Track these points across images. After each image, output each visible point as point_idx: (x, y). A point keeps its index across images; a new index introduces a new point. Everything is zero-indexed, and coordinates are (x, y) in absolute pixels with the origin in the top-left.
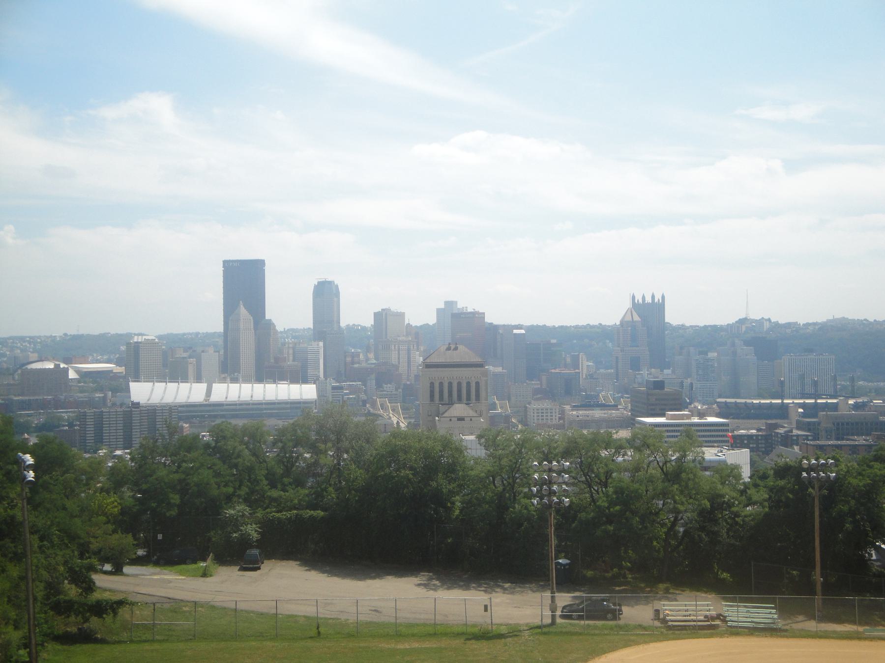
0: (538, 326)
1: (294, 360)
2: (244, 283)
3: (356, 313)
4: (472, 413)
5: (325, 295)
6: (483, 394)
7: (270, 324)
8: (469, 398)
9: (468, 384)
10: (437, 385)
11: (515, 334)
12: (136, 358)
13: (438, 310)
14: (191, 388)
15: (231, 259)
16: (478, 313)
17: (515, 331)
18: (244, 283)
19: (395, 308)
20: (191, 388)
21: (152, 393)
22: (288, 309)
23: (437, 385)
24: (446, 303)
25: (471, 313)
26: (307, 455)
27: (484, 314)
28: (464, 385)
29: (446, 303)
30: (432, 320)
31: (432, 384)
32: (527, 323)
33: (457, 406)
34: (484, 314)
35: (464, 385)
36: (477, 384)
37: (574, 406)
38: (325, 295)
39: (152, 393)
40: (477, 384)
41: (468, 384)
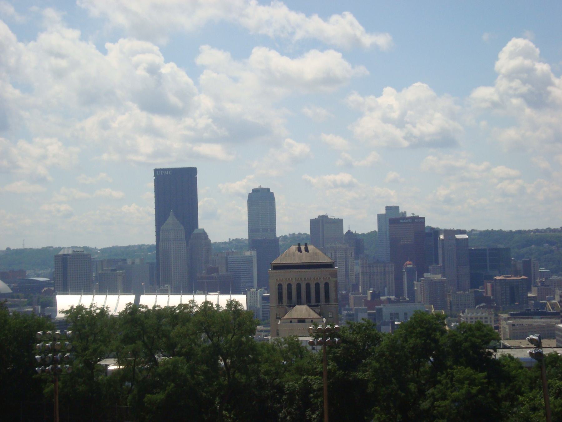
0: (493, 231)
1: (227, 271)
2: (176, 191)
3: (292, 221)
4: (314, 315)
5: (261, 202)
6: (332, 295)
7: (204, 235)
8: (318, 300)
9: (317, 285)
10: (285, 287)
11: (458, 240)
12: (77, 269)
13: (380, 217)
14: (169, 300)
15: (162, 167)
16: (418, 218)
17: (458, 236)
18: (176, 191)
19: (333, 214)
20: (169, 300)
21: (117, 304)
22: (222, 219)
23: (285, 287)
24: (388, 208)
25: (410, 218)
26: (222, 363)
27: (424, 218)
28: (313, 287)
29: (388, 208)
30: (374, 227)
31: (280, 286)
32: (468, 229)
33: (298, 307)
34: (424, 218)
35: (313, 287)
36: (327, 285)
37: (512, 315)
38: (261, 202)
39: (117, 304)
40: (327, 285)
41: (317, 285)
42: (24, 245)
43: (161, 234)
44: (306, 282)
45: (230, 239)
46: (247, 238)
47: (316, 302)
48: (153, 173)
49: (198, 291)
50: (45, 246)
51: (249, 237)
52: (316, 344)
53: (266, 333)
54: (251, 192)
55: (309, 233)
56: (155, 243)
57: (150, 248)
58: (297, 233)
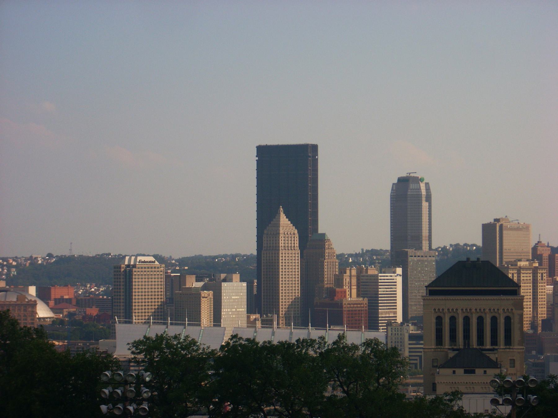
5: (407, 199)
22: (354, 218)
31: (439, 320)
42: (71, 250)
43: (264, 239)
44: (451, 314)
45: (362, 250)
46: (388, 247)
47: (492, 345)
48: (316, 144)
49: (27, 331)
50: (101, 253)
51: (391, 247)
52: (501, 403)
53: (415, 388)
54: (396, 181)
55: (479, 243)
56: (255, 253)
57: (249, 258)
58: (462, 244)
